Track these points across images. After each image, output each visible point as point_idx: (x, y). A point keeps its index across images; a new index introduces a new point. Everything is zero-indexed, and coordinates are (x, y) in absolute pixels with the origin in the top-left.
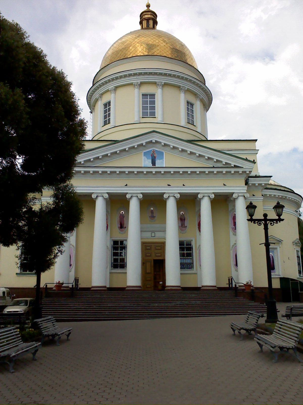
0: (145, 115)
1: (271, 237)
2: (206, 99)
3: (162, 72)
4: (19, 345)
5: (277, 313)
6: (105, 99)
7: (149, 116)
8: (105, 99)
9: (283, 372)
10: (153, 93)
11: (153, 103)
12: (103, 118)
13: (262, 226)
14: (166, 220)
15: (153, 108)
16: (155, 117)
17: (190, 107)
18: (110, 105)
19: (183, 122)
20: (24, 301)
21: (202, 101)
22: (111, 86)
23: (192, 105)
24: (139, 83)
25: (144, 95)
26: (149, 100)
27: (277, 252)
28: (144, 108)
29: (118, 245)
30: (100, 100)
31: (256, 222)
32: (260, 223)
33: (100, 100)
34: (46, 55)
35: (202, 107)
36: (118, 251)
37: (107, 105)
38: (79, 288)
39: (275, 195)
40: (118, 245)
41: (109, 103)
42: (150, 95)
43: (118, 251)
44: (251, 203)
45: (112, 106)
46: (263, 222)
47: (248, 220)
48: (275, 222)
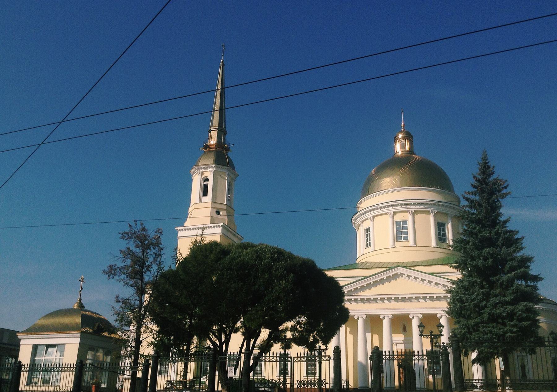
0: (398, 239)
3: (416, 202)
5: (219, 390)
6: (366, 225)
8: (366, 225)
9: (69, 387)
11: (406, 228)
12: (365, 242)
13: (429, 340)
16: (408, 241)
19: (433, 243)
20: (496, 378)
22: (370, 215)
24: (392, 213)
25: (398, 223)
31: (425, 336)
32: (427, 338)
37: (368, 230)
38: (229, 377)
42: (403, 221)
45: (371, 232)
46: (430, 336)
47: (419, 335)
48: (438, 336)
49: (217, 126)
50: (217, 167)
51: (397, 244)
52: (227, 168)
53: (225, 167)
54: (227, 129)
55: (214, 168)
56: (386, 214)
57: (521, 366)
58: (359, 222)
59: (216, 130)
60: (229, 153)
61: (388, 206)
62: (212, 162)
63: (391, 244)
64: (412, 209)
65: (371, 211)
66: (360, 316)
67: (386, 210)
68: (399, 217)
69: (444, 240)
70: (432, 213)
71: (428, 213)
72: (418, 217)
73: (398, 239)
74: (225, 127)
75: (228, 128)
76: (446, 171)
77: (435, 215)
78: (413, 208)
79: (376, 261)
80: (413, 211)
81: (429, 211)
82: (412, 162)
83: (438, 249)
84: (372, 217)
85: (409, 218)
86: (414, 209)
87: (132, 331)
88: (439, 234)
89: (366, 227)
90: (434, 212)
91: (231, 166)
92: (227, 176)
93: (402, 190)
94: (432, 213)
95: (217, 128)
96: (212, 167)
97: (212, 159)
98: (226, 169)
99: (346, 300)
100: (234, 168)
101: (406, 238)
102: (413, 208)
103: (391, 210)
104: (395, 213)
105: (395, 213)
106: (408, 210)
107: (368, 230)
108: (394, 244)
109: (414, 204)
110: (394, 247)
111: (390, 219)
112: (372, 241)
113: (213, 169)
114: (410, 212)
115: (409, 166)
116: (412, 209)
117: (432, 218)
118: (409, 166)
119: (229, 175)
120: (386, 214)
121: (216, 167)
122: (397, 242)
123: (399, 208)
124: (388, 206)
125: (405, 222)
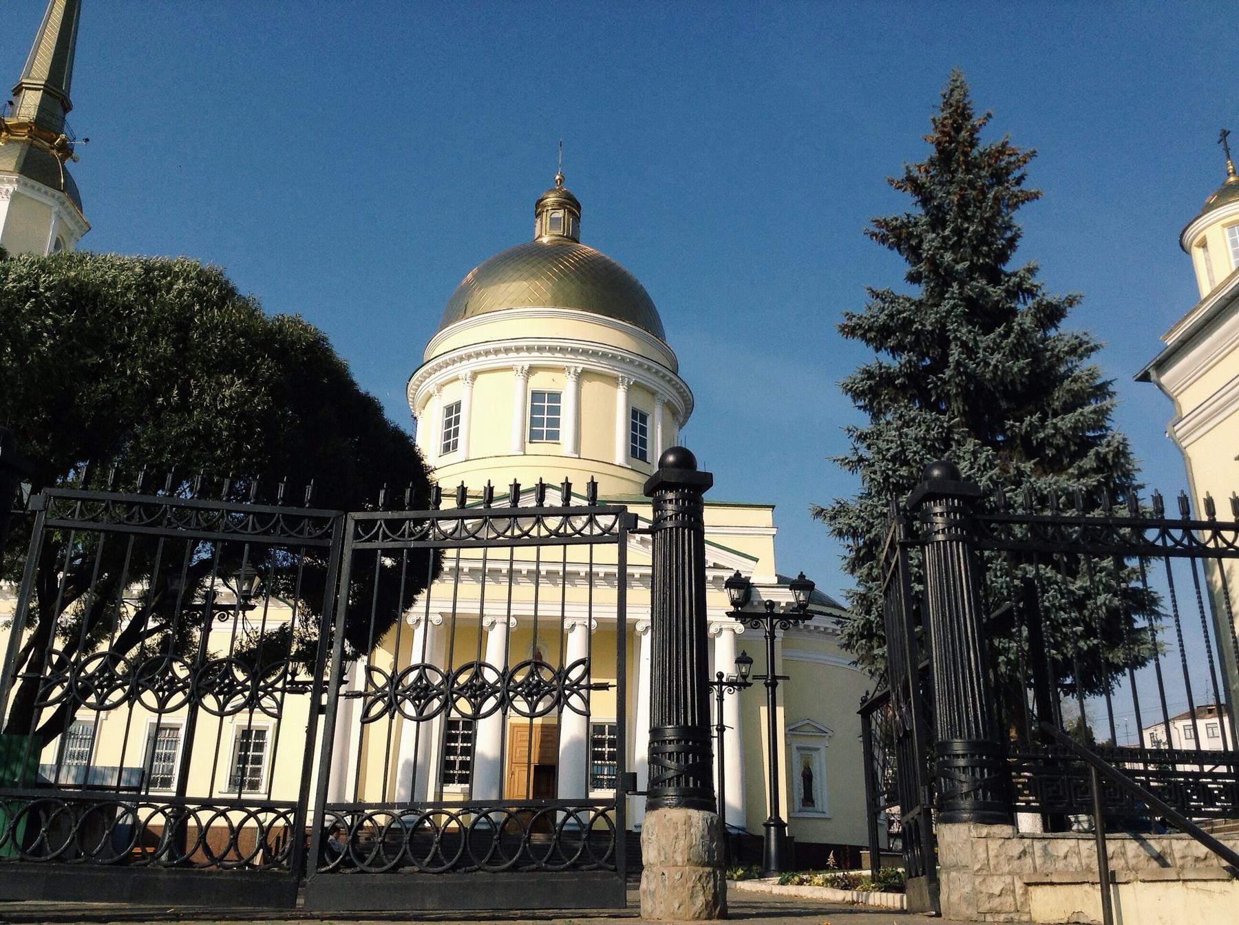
1: (806, 722)
2: (679, 404)
4: (1222, 145)
6: (450, 396)
7: (545, 441)
10: (570, 311)
11: (556, 411)
14: (1196, 281)
15: (556, 423)
17: (638, 422)
18: (458, 410)
19: (620, 456)
21: (668, 405)
22: (465, 369)
23: (644, 418)
24: (526, 368)
25: (537, 396)
26: (545, 416)
27: (820, 756)
28: (534, 422)
29: (458, 730)
30: (438, 396)
33: (438, 396)
34: (368, 393)
35: (669, 416)
36: (457, 744)
37: (453, 411)
39: (826, 629)
40: (458, 730)
41: (458, 406)
43: (457, 744)
44: (744, 654)
45: (463, 414)
49: (42, 79)
50: (26, 184)
51: (531, 448)
52: (58, 194)
53: (51, 191)
54: (73, 97)
55: (16, 186)
56: (509, 369)
57: (804, 775)
58: (430, 385)
59: (39, 89)
60: (68, 163)
61: (518, 350)
62: (11, 168)
63: (515, 447)
64: (576, 365)
65: (469, 357)
66: (578, 622)
67: (512, 359)
68: (541, 382)
69: (643, 456)
70: (623, 382)
71: (614, 381)
72: (589, 387)
73: (535, 436)
74: (69, 84)
75: (77, 93)
76: (650, 294)
77: (630, 390)
78: (581, 363)
79: (1212, 260)
80: (579, 371)
81: (616, 378)
82: (569, 262)
83: (629, 471)
84: (469, 374)
85: (565, 385)
86: (668, 397)
87: (992, 854)
88: (634, 439)
89: (450, 401)
90: (628, 382)
91: (71, 190)
92: (53, 217)
93: (552, 315)
94: (623, 382)
95: (43, 83)
96: (10, 182)
97: (14, 161)
98: (53, 196)
99: (466, 570)
100: (77, 202)
101: (554, 436)
102: (581, 363)
103: (526, 360)
104: (532, 370)
105: (532, 370)
106: (568, 364)
107: (453, 411)
108: (523, 448)
109: (585, 352)
110: (522, 453)
111: (519, 381)
112: (462, 438)
113: (11, 188)
114: (572, 370)
115: (561, 270)
116: (576, 365)
117: (621, 394)
118: (561, 270)
119: (59, 217)
120: (509, 369)
121: (21, 182)
122: (530, 442)
123: (545, 359)
124: (518, 350)
125: (555, 397)
